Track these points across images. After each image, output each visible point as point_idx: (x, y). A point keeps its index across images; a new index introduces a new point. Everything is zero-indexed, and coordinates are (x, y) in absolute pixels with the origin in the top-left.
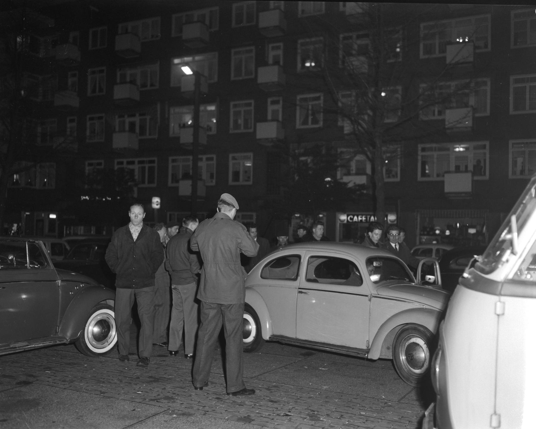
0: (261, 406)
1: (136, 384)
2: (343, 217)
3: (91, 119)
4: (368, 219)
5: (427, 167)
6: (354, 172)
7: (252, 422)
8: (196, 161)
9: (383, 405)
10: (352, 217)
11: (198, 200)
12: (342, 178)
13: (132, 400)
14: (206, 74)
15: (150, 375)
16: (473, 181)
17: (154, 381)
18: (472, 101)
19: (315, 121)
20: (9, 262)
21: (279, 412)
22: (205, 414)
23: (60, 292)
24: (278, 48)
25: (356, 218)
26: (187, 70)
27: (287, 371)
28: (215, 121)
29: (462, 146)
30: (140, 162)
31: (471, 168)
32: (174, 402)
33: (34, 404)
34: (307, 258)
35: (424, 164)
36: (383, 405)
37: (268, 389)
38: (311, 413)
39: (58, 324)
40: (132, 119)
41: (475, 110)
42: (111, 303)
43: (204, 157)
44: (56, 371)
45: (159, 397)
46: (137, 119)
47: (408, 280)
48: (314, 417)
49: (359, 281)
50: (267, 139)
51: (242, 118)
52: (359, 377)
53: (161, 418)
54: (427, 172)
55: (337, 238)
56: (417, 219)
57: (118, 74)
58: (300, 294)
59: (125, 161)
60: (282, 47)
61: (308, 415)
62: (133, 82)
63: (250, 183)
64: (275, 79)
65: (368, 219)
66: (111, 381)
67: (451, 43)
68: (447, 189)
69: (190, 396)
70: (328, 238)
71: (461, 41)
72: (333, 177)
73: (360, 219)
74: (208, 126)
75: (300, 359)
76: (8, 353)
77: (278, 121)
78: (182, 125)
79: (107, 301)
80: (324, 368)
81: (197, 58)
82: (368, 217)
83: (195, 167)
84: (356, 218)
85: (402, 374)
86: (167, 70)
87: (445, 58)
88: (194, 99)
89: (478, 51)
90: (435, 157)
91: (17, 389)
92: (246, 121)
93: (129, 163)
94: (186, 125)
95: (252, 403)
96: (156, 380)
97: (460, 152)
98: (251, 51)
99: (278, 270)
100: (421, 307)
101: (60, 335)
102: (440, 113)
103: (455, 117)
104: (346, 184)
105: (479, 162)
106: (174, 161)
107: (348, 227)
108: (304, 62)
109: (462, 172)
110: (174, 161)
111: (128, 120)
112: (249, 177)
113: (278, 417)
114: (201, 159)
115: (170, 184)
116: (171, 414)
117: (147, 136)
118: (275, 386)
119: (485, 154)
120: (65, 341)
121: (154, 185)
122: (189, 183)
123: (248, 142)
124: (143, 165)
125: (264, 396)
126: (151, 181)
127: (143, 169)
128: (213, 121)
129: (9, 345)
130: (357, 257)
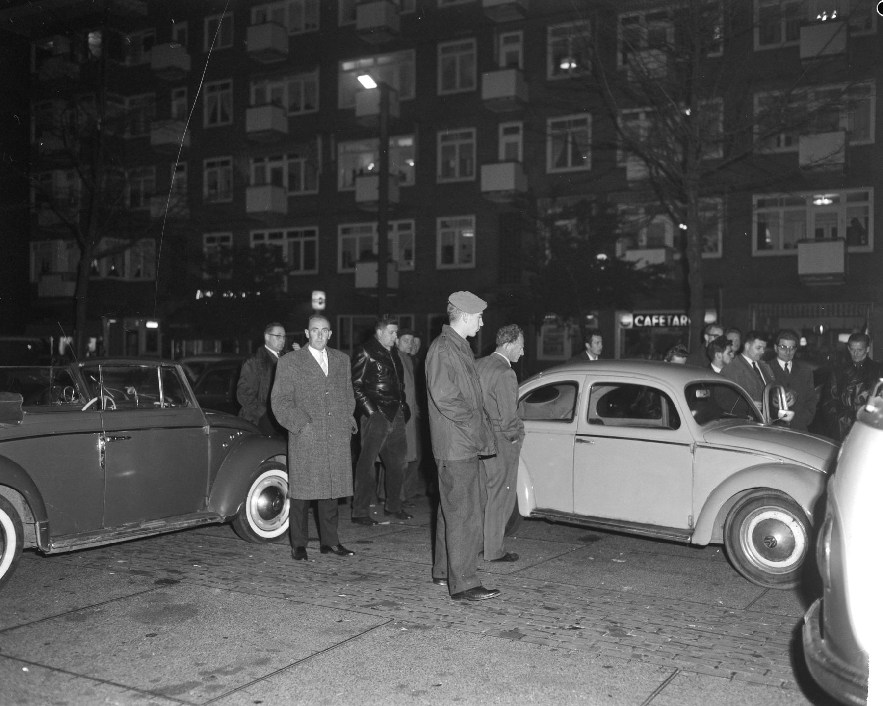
0: (532, 615)
1: (335, 584)
2: (627, 319)
3: (211, 165)
4: (669, 320)
5: (768, 233)
6: (644, 243)
7: (523, 639)
8: (383, 230)
9: (721, 614)
10: (642, 318)
11: (388, 295)
12: (624, 255)
13: (334, 607)
14: (396, 85)
15: (352, 569)
16: (846, 255)
17: (360, 579)
18: (845, 122)
19: (577, 161)
20: (127, 398)
21: (562, 624)
22: (449, 627)
23: (209, 444)
24: (515, 39)
25: (648, 319)
26: (367, 82)
27: (562, 563)
28: (412, 164)
29: (827, 196)
30: (290, 235)
31: (842, 233)
32: (398, 609)
33: (189, 611)
34: (589, 386)
35: (762, 228)
36: (721, 614)
37: (538, 591)
38: (612, 625)
39: (207, 493)
40: (276, 164)
41: (849, 135)
42: (282, 459)
43: (395, 224)
44: (208, 564)
45: (374, 602)
46: (284, 164)
47: (751, 418)
48: (617, 631)
49: (675, 422)
50: (499, 192)
51: (457, 156)
52: (678, 573)
53: (384, 633)
54: (768, 240)
55: (618, 354)
56: (751, 320)
57: (253, 89)
58: (579, 445)
59: (266, 232)
60: (521, 38)
61: (607, 628)
62: (276, 103)
63: (472, 265)
64: (511, 92)
65: (669, 320)
66: (297, 580)
67: (806, 23)
68: (802, 269)
69: (421, 600)
70: (607, 356)
71: (824, 18)
72: (610, 252)
73: (655, 321)
74: (400, 172)
75: (579, 546)
76: (137, 537)
77: (515, 161)
78: (358, 172)
79: (277, 457)
80: (619, 559)
81: (382, 59)
82: (669, 318)
83: (384, 242)
84: (648, 319)
85: (745, 570)
86: (331, 80)
87: (797, 49)
88: (380, 128)
89: (853, 35)
90: (782, 215)
91: (159, 591)
92: (463, 163)
93: (273, 236)
94: (365, 172)
95: (518, 611)
96: (365, 578)
97: (823, 205)
98: (470, 46)
99: (537, 406)
100: (777, 461)
101: (210, 509)
102: (789, 142)
103: (816, 149)
104: (632, 264)
105: (855, 221)
106: (345, 231)
107: (634, 335)
108: (558, 63)
109: (827, 240)
110: (345, 231)
111: (269, 166)
112: (469, 256)
113: (561, 631)
114: (391, 228)
115: (340, 269)
116: (398, 627)
117: (302, 192)
118: (547, 587)
119: (866, 209)
120: (218, 520)
121: (315, 272)
122: (373, 266)
123: (467, 198)
124: (296, 239)
125: (534, 600)
126: (309, 265)
127: (297, 245)
128: (408, 165)
129: (138, 526)
130: (671, 384)
